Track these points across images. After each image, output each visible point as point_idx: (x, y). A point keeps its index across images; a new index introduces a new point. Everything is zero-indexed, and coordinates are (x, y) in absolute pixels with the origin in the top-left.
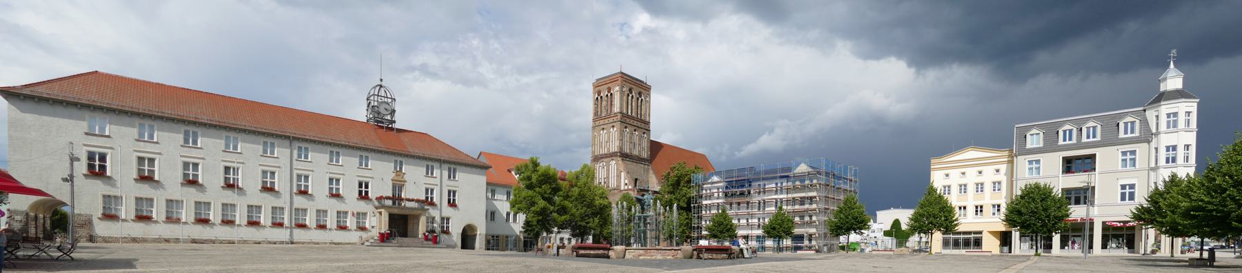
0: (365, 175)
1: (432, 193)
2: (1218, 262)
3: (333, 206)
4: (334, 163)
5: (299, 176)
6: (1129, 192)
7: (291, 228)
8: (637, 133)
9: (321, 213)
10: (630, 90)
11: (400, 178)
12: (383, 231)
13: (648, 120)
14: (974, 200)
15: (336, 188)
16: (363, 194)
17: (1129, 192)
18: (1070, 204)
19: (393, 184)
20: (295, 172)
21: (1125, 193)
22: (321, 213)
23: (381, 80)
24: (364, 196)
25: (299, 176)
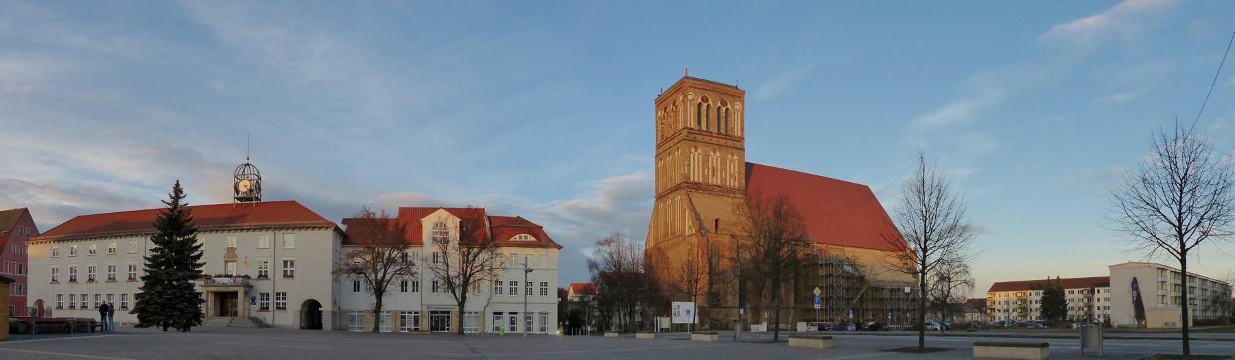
8: (718, 154)
10: (705, 99)
13: (737, 133)
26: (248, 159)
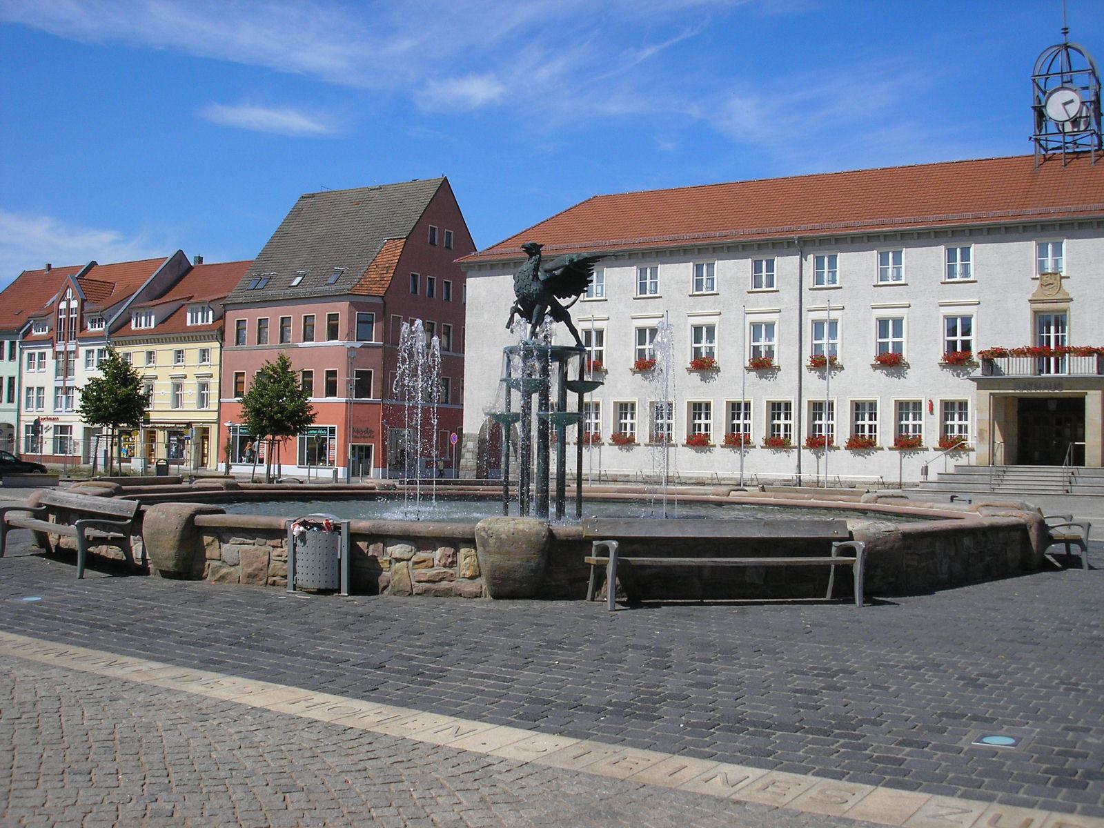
0: (959, 300)
1: (967, 331)
2: (552, 259)
3: (691, 388)
4: (764, 289)
5: (818, 325)
6: (955, 335)
7: (799, 448)
9: (625, 409)
11: (1051, 294)
12: (596, 450)
14: (853, 602)
15: (963, 342)
16: (959, 349)
17: (955, 335)
18: (311, 396)
19: (1036, 312)
20: (809, 318)
21: (644, 350)
22: (737, 409)
23: (1065, 31)
24: (957, 358)
25: (818, 325)
26: (1065, 31)
